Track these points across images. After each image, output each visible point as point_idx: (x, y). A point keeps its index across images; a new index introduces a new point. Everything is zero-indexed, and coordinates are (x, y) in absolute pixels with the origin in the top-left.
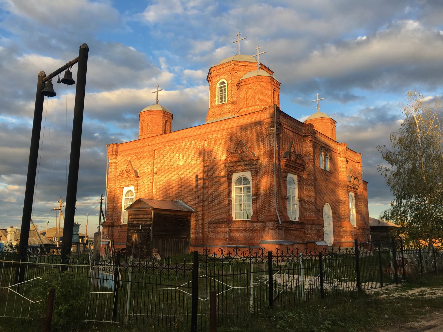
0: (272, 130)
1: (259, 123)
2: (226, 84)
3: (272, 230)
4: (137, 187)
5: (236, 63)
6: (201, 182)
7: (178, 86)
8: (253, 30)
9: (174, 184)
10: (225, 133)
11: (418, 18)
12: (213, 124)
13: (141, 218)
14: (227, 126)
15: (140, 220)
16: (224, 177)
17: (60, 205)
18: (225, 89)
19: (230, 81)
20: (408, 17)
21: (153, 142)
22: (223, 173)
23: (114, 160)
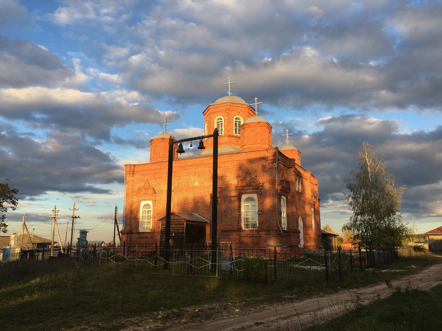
0: (274, 165)
1: (264, 159)
2: (223, 120)
4: (154, 201)
7: (93, 89)
8: (167, 42)
9: (190, 201)
11: (316, 46)
14: (237, 159)
16: (235, 197)
17: (54, 214)
18: (222, 124)
19: (226, 118)
20: (307, 43)
22: (234, 194)
23: (131, 178)
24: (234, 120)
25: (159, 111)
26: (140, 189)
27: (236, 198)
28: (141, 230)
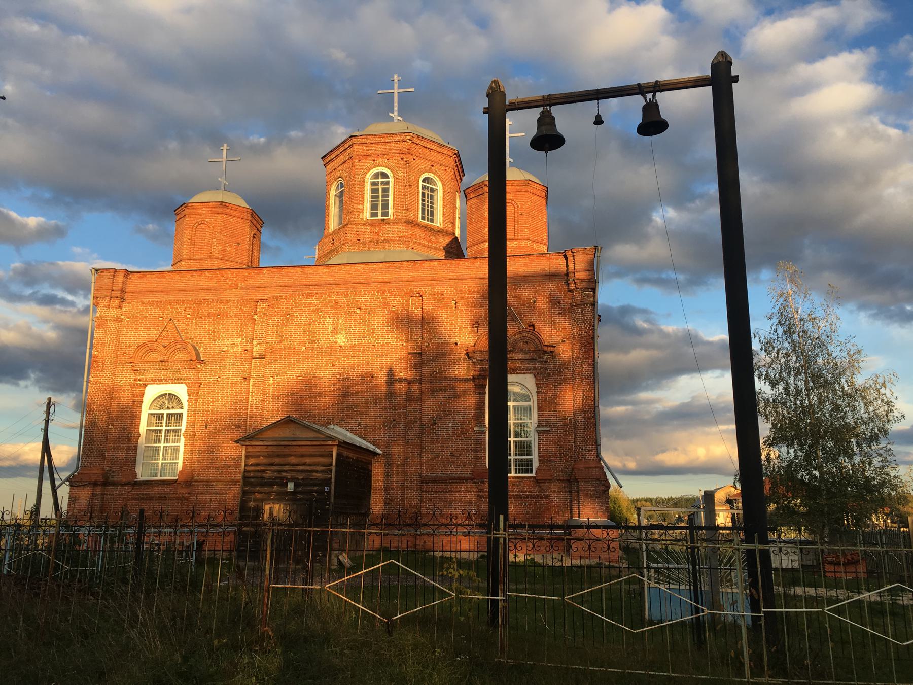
0: (588, 296)
2: (391, 180)
3: (591, 497)
4: (195, 387)
5: (415, 140)
6: (400, 388)
12: (436, 263)
13: (293, 465)
15: (287, 468)
16: (466, 380)
18: (386, 191)
19: (401, 175)
21: (251, 281)
24: (421, 183)
25: (14, 215)
26: (146, 347)
27: (470, 384)
28: (142, 474)
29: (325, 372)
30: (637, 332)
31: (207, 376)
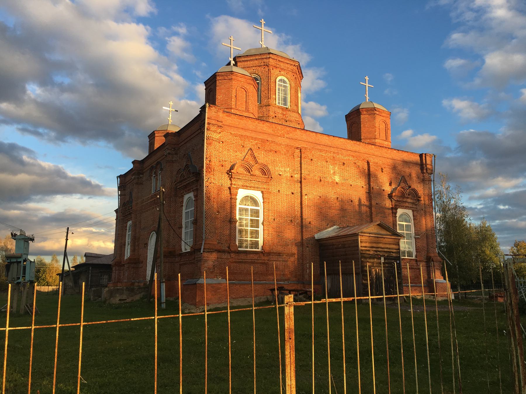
10: (390, 162)
15: (380, 250)
16: (389, 209)
29: (332, 194)
30: (22, 163)
31: (274, 189)
